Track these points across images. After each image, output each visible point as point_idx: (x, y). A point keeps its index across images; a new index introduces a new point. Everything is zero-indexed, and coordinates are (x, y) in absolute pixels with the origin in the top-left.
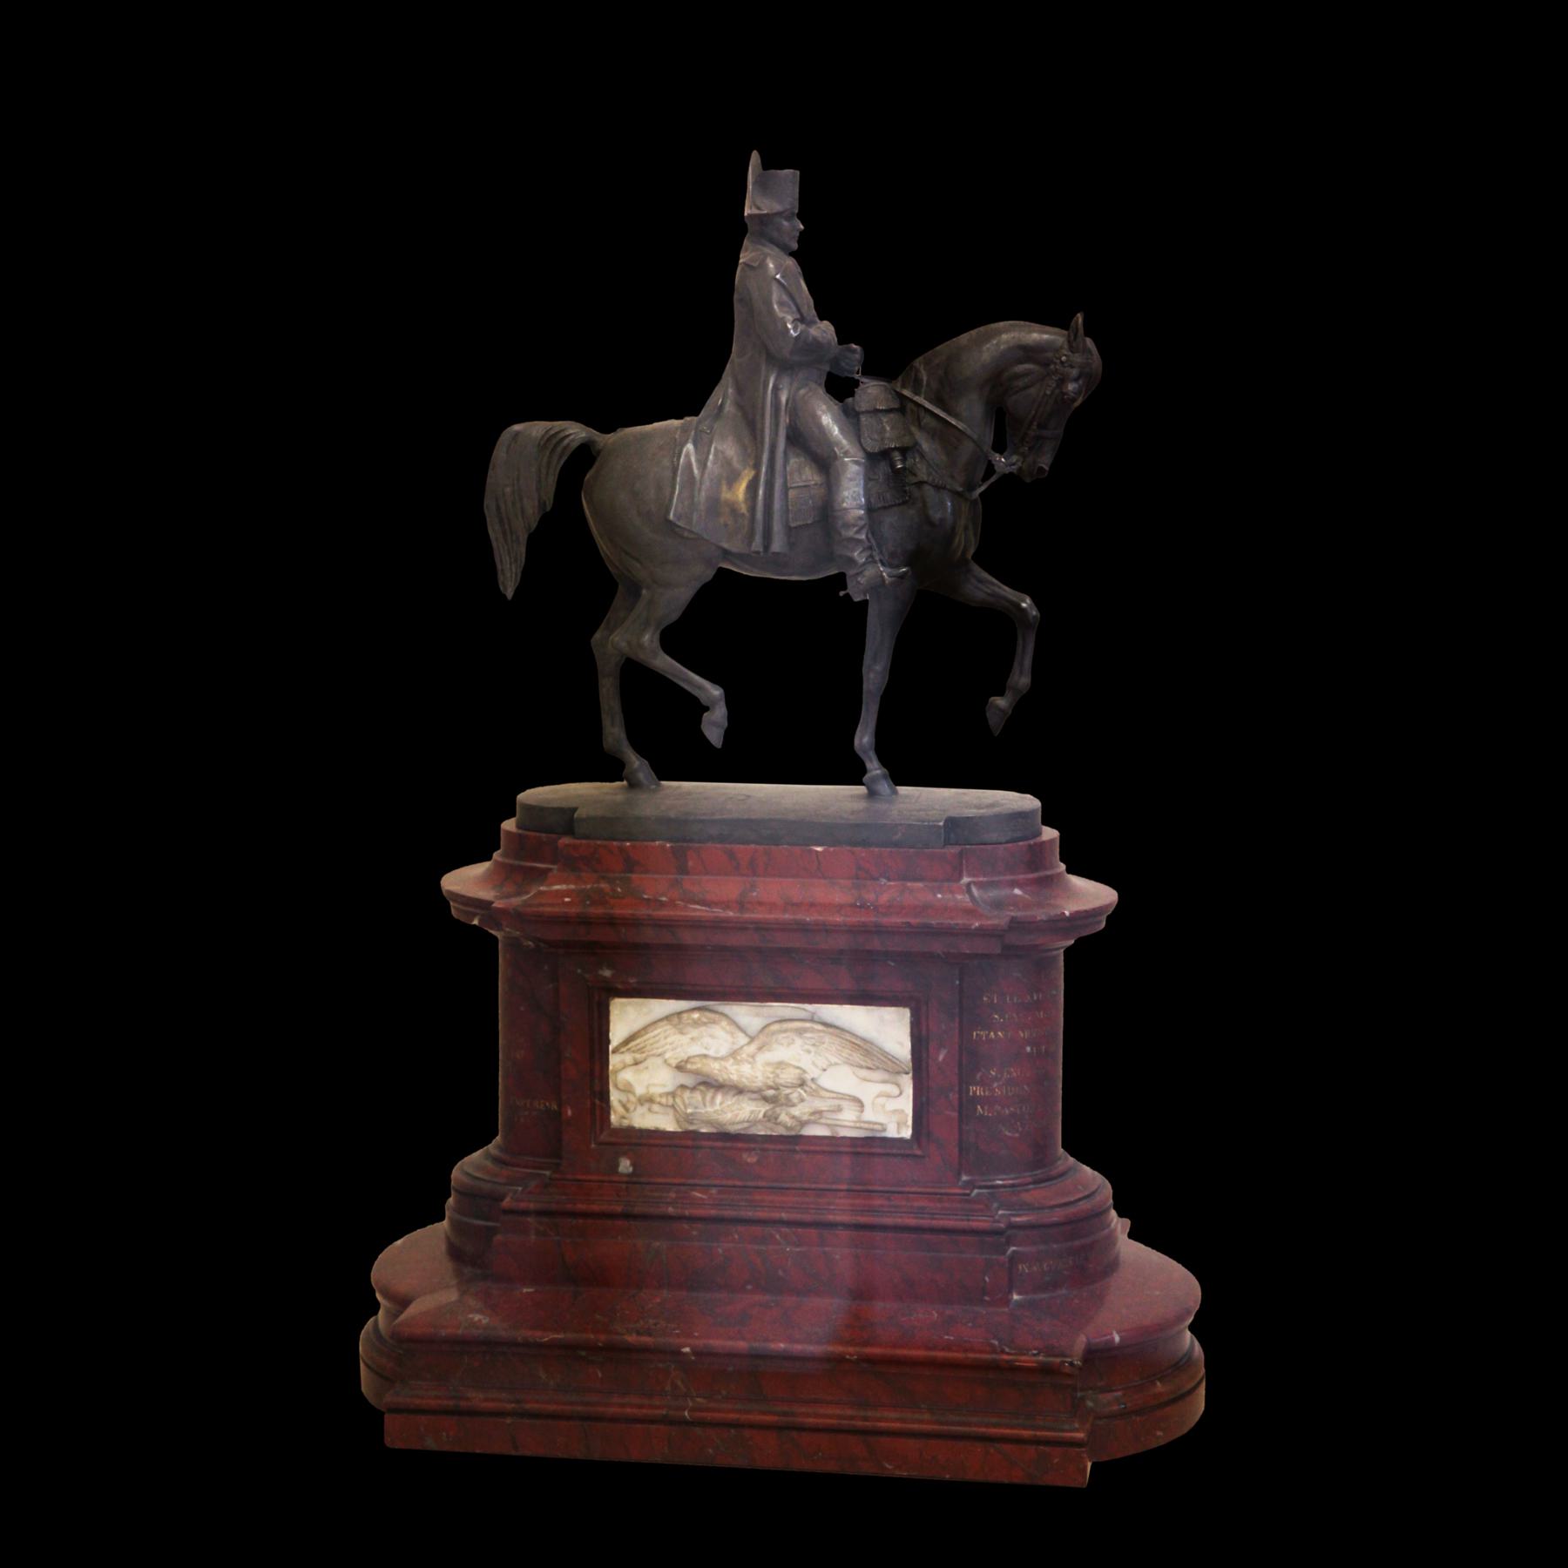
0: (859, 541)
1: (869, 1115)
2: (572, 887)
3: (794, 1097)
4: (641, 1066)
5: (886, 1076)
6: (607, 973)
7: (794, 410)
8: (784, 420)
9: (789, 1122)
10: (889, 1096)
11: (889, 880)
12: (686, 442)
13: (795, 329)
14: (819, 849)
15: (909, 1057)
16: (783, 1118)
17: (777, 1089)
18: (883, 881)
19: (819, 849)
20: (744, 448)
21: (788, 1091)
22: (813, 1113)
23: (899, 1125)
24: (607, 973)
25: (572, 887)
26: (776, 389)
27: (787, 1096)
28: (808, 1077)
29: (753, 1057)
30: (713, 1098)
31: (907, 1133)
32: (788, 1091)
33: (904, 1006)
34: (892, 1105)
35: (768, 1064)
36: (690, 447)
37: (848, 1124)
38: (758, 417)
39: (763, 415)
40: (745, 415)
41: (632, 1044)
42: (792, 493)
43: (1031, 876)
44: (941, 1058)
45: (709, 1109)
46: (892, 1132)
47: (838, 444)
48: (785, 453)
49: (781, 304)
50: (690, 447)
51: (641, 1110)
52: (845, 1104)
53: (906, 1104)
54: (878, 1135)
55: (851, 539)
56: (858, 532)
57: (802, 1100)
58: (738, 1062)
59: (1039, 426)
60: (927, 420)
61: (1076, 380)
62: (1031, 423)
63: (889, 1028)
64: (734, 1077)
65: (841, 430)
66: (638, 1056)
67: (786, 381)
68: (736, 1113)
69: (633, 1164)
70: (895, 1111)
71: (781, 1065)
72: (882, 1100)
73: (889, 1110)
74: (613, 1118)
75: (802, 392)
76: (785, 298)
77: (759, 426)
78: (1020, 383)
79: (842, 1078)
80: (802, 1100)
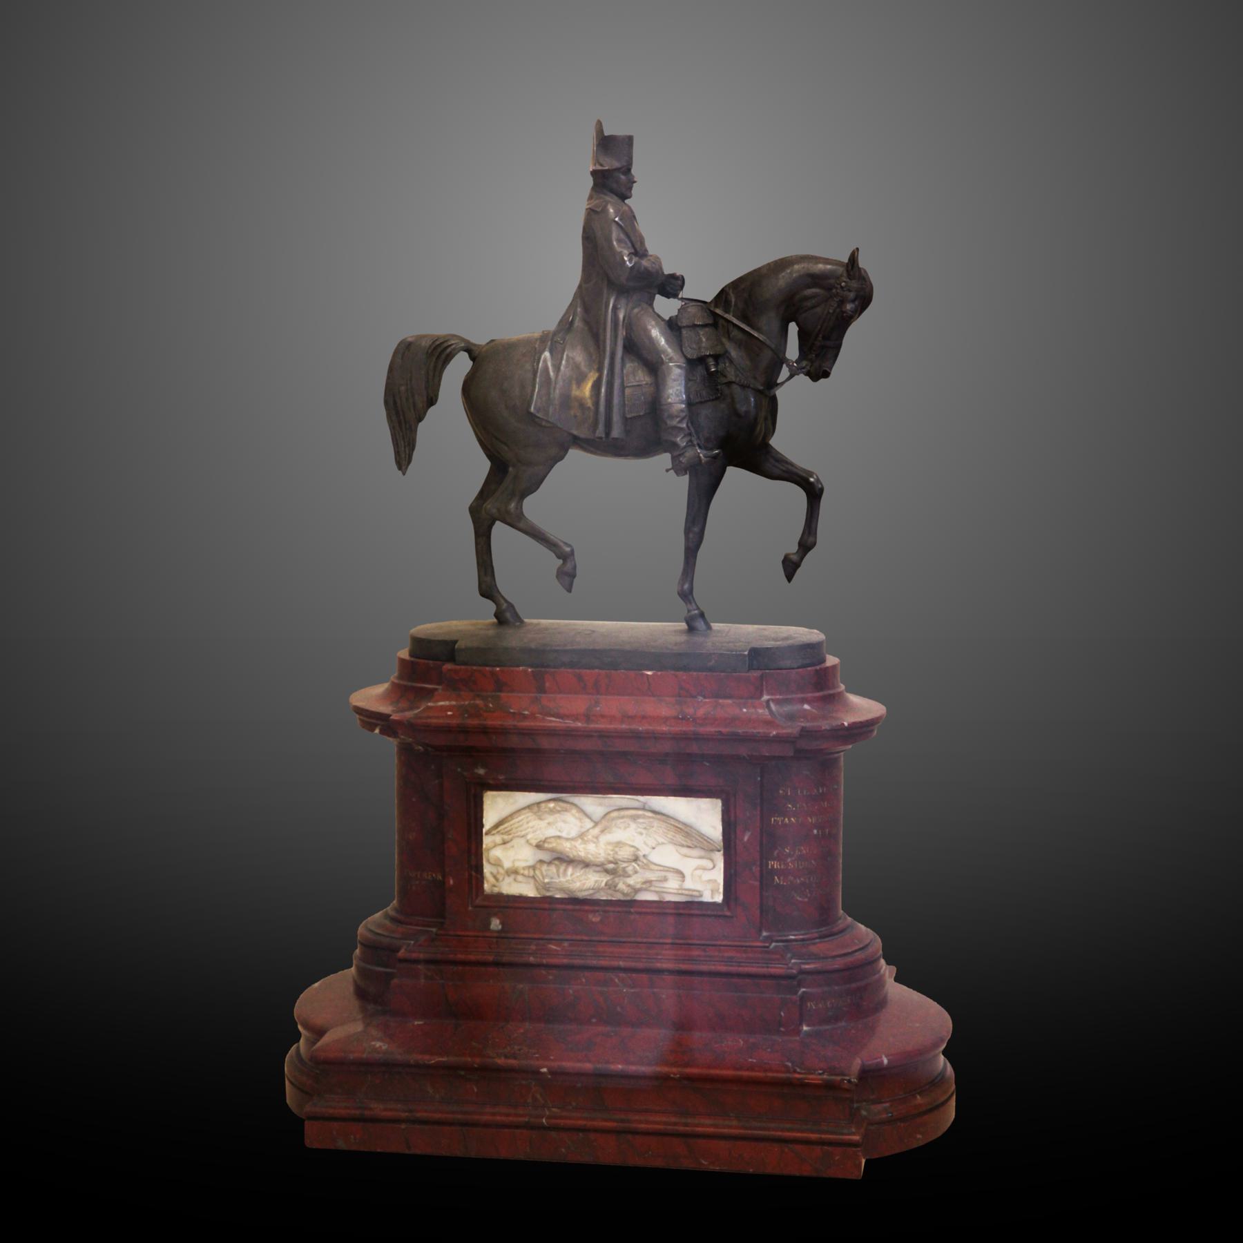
0: (681, 429)
1: (689, 884)
2: (454, 703)
3: (630, 869)
4: (508, 845)
5: (702, 853)
6: (481, 771)
7: (629, 325)
8: (622, 333)
9: (626, 890)
10: (705, 869)
11: (705, 697)
12: (544, 351)
13: (630, 260)
14: (649, 673)
15: (721, 838)
16: (621, 886)
17: (616, 863)
18: (700, 698)
19: (649, 673)
20: (590, 355)
21: (625, 865)
22: (645, 883)
23: (713, 892)
24: (481, 771)
25: (454, 703)
26: (615, 308)
27: (624, 869)
28: (641, 854)
29: (597, 838)
30: (565, 870)
31: (719, 898)
32: (625, 865)
33: (717, 797)
34: (707, 876)
35: (609, 844)
36: (547, 354)
37: (672, 891)
38: (601, 331)
39: (605, 329)
40: (590, 329)
41: (501, 828)
44: (746, 838)
45: (562, 879)
46: (707, 898)
47: (664, 352)
48: (623, 359)
49: (619, 241)
50: (547, 354)
51: (508, 880)
52: (670, 875)
53: (718, 875)
54: (696, 900)
55: (675, 428)
56: (680, 422)
57: (636, 872)
58: (585, 842)
59: (824, 338)
60: (735, 333)
61: (853, 301)
62: (817, 335)
63: (705, 815)
64: (582, 854)
65: (667, 341)
66: (506, 837)
67: (623, 302)
68: (583, 883)
69: (502, 923)
70: (709, 881)
71: (619, 844)
72: (699, 872)
73: (705, 880)
74: (486, 886)
75: (636, 310)
76: (622, 236)
77: (601, 337)
78: (809, 304)
79: (667, 855)
80: (636, 872)
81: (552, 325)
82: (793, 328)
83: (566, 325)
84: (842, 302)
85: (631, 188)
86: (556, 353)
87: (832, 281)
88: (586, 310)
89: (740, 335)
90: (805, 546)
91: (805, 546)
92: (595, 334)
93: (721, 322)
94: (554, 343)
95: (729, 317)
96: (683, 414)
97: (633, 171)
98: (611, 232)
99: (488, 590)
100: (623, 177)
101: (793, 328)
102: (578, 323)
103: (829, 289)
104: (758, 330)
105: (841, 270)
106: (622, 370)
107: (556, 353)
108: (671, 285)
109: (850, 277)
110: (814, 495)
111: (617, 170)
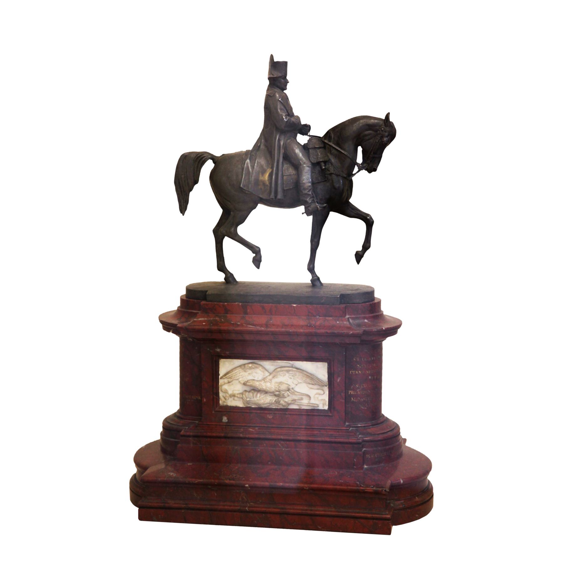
0: (309, 195)
1: (313, 401)
3: (286, 395)
4: (231, 384)
5: (319, 387)
6: (218, 350)
8: (282, 151)
9: (284, 404)
10: (320, 394)
11: (320, 316)
12: (247, 159)
13: (286, 118)
14: (295, 305)
15: (327, 380)
16: (282, 402)
17: (279, 392)
18: (318, 317)
19: (295, 305)
20: (268, 161)
21: (283, 392)
22: (293, 400)
23: (324, 405)
24: (218, 350)
26: (279, 140)
27: (283, 394)
28: (291, 387)
29: (271, 380)
30: (256, 395)
31: (326, 408)
32: (283, 392)
33: (325, 362)
34: (321, 397)
35: (276, 383)
36: (248, 161)
37: (305, 404)
38: (273, 150)
39: (274, 149)
40: (268, 149)
41: (227, 376)
42: (285, 177)
43: (371, 315)
44: (338, 380)
45: (255, 399)
46: (321, 407)
47: (301, 160)
48: (282, 163)
49: (281, 109)
50: (248, 161)
51: (231, 399)
52: (304, 397)
53: (326, 397)
54: (316, 408)
55: (306, 194)
56: (309, 191)
57: (289, 396)
58: (265, 382)
59: (374, 153)
60: (333, 151)
61: (387, 137)
62: (371, 152)
63: (320, 370)
64: (264, 388)
65: (303, 155)
66: (229, 380)
67: (283, 137)
68: (265, 400)
69: (228, 419)
70: (322, 400)
71: (281, 383)
72: (317, 396)
73: (320, 399)
74: (221, 402)
75: (289, 141)
76: (282, 107)
77: (273, 153)
78: (367, 138)
79: (303, 388)
80: (289, 396)
81: (249, 146)
82: (360, 149)
83: (257, 147)
84: (382, 137)
85: (286, 85)
86: (252, 160)
87: (378, 128)
88: (266, 140)
89: (336, 152)
90: (366, 245)
91: (366, 245)
92: (270, 152)
93: (327, 146)
94: (251, 156)
95: (331, 144)
96: (310, 188)
97: (287, 78)
98: (277, 105)
99: (311, 268)
100: (283, 80)
101: (360, 149)
102: (262, 147)
103: (376, 131)
104: (344, 150)
105: (382, 122)
106: (282, 168)
107: (252, 160)
108: (305, 130)
109: (386, 126)
110: (369, 222)
111: (280, 77)
